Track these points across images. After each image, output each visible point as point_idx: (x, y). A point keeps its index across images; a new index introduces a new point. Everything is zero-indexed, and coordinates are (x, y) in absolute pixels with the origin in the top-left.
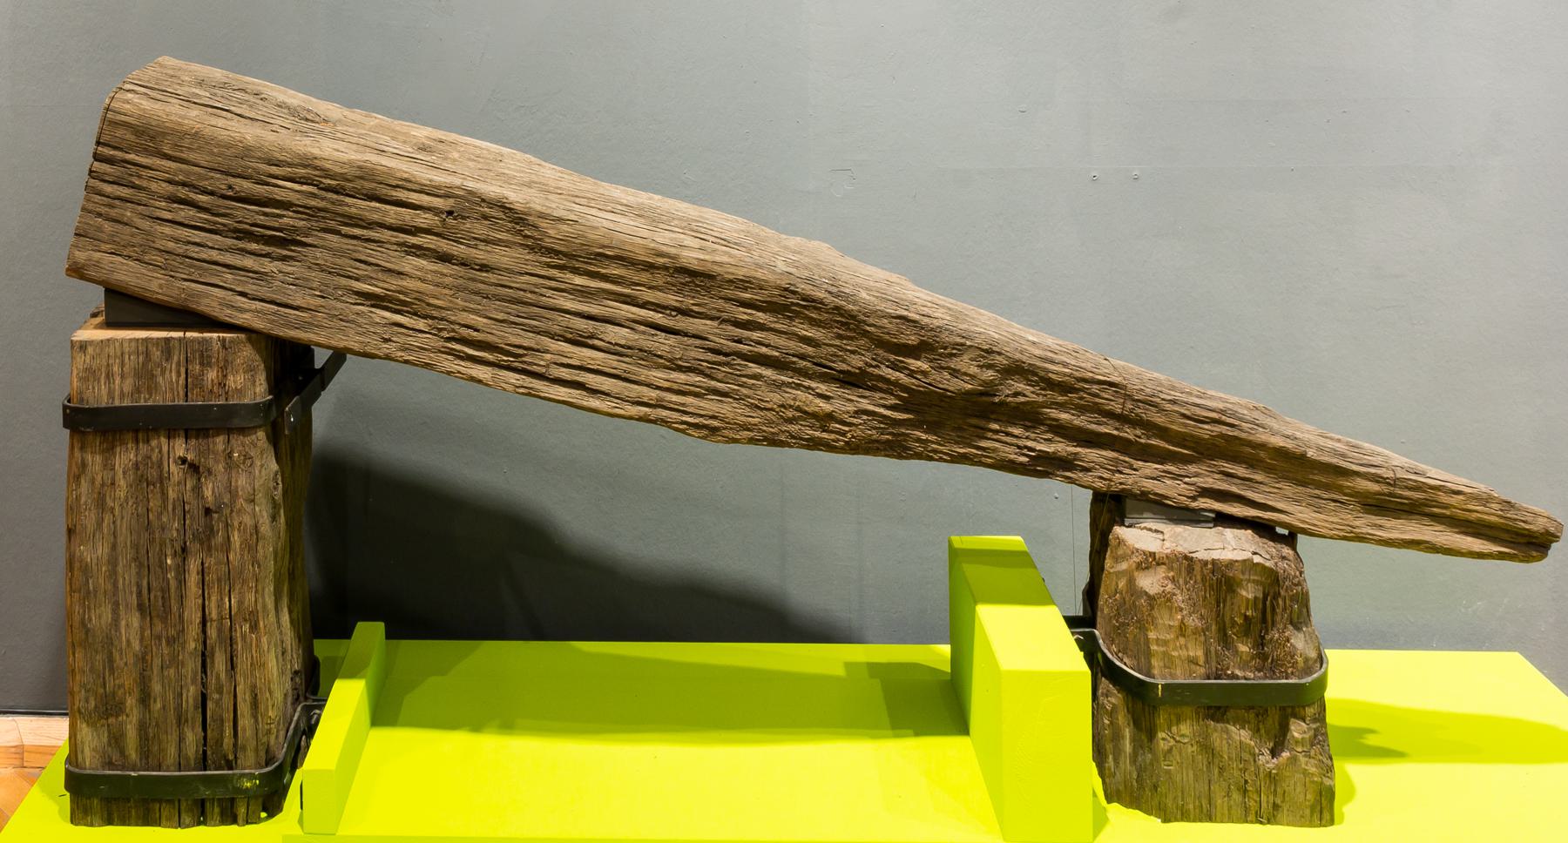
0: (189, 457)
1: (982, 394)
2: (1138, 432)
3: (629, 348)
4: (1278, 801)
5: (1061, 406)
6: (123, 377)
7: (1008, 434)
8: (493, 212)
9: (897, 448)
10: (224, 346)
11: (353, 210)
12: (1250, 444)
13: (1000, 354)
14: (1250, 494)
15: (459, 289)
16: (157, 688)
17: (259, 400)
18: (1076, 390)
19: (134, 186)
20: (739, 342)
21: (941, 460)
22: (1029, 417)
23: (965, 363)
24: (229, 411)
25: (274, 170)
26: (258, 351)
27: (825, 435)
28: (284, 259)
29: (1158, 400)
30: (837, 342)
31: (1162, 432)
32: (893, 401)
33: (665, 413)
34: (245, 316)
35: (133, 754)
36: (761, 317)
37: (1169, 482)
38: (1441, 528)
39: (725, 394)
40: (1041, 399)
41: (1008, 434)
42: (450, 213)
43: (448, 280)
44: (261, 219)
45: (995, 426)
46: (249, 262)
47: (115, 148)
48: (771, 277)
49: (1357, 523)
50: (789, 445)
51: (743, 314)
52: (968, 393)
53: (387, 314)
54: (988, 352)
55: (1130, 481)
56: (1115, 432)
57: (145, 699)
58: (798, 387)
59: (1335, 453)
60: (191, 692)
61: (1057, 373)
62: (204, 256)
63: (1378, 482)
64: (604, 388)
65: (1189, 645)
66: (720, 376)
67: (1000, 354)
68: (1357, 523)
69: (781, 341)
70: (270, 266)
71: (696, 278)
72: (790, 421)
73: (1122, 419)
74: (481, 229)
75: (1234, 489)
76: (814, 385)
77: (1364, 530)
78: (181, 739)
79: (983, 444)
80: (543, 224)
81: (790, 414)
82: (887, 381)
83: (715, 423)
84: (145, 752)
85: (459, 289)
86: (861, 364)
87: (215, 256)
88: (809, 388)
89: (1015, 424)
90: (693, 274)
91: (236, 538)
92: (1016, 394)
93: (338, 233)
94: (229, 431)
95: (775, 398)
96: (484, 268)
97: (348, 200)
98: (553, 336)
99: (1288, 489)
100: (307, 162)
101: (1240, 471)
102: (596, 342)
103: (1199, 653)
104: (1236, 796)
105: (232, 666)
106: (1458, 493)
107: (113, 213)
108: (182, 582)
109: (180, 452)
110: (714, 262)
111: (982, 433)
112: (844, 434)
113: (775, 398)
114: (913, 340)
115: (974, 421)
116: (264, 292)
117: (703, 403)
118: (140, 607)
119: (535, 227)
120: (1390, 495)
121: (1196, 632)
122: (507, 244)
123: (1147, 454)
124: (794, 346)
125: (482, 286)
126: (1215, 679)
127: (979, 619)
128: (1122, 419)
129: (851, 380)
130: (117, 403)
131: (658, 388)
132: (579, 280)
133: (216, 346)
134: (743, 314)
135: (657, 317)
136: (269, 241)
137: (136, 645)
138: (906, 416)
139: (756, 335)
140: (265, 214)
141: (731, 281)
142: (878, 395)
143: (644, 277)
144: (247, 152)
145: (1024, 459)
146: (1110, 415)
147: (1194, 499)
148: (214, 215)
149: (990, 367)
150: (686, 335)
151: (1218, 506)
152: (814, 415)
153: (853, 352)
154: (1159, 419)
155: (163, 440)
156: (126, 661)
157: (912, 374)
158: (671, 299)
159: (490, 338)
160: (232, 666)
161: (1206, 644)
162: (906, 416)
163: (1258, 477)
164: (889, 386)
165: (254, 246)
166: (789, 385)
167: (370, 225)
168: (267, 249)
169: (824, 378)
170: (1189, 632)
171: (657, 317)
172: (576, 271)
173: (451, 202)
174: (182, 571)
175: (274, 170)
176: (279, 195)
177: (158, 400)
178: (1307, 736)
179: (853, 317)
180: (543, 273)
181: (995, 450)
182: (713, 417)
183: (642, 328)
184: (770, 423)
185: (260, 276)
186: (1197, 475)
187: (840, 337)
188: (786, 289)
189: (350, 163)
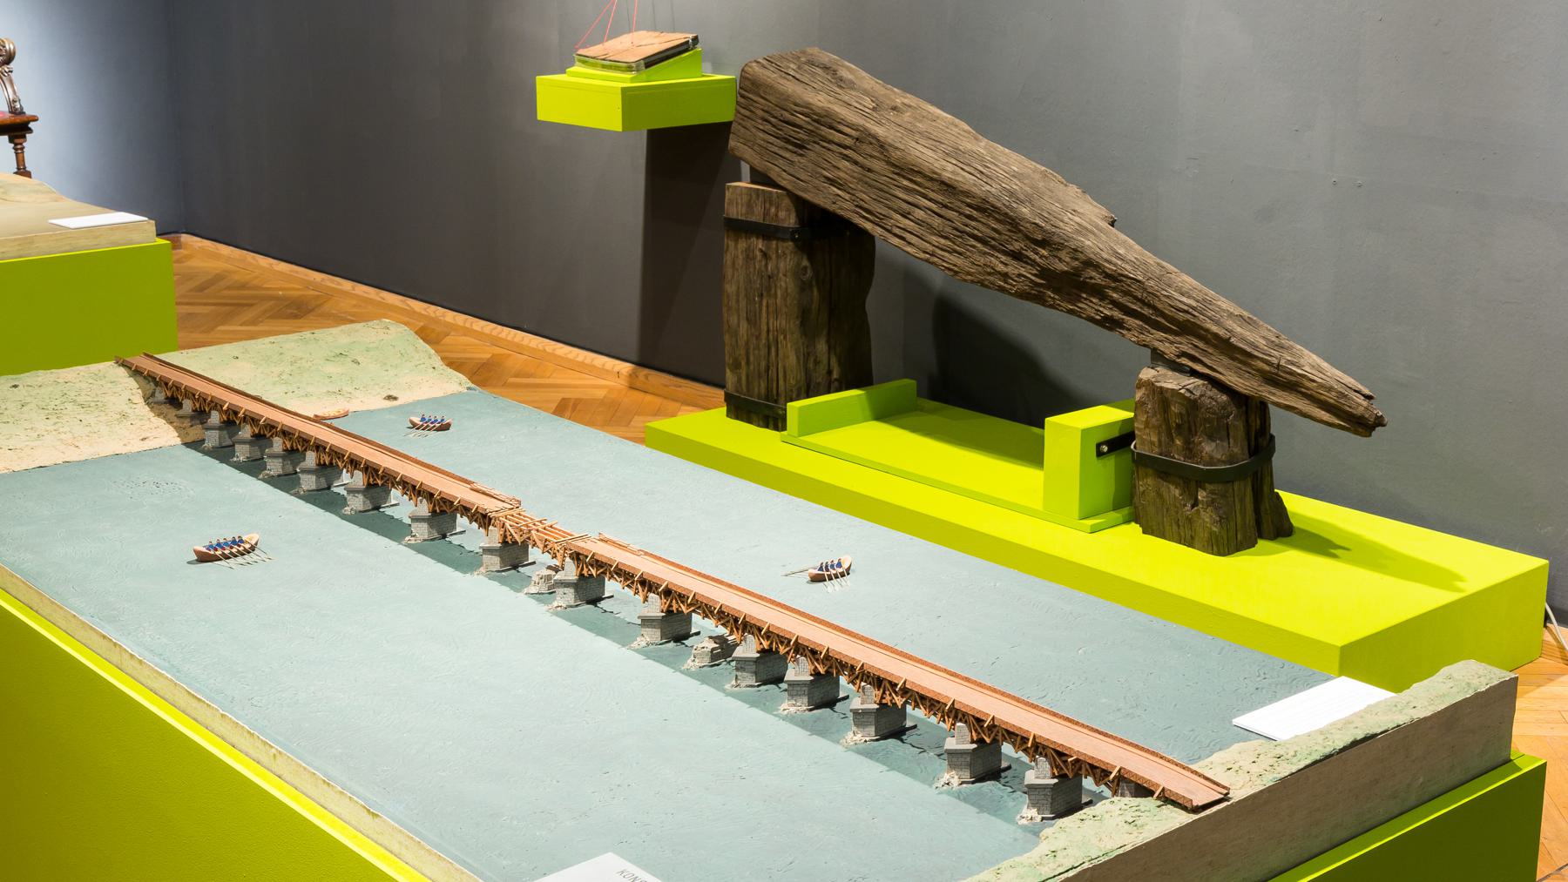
0: (764, 249)
1: (1074, 275)
2: (1151, 312)
3: (924, 222)
4: (1193, 534)
5: (1114, 289)
6: (742, 205)
7: (1091, 302)
8: (874, 141)
9: (1039, 299)
10: (778, 197)
11: (823, 133)
12: (1202, 328)
13: (1082, 253)
14: (1204, 359)
15: (860, 180)
16: (752, 359)
17: (791, 226)
18: (1120, 281)
19: (751, 111)
20: (966, 226)
21: (1062, 310)
22: (1098, 292)
23: (1063, 254)
24: (777, 229)
25: (797, 108)
26: (792, 202)
27: (1006, 285)
28: (801, 155)
29: (1158, 294)
30: (1007, 233)
31: (1163, 315)
32: (1035, 272)
33: (936, 259)
34: (784, 182)
35: (745, 390)
36: (975, 213)
37: (1167, 344)
38: (1308, 402)
39: (960, 254)
40: (1103, 283)
41: (1091, 302)
42: (857, 139)
43: (855, 175)
44: (792, 133)
45: (1084, 296)
46: (787, 155)
47: (745, 91)
48: (978, 192)
49: (1260, 389)
50: (989, 288)
51: (968, 211)
52: (1066, 272)
53: (835, 189)
54: (1076, 250)
55: (1148, 340)
56: (1139, 310)
57: (748, 363)
58: (992, 256)
59: (1252, 344)
60: (763, 364)
61: (1109, 269)
62: (773, 150)
63: (1269, 365)
64: (912, 242)
65: (1151, 433)
66: (958, 243)
67: (1082, 253)
68: (1260, 389)
69: (984, 229)
70: (796, 159)
71: (948, 187)
72: (989, 274)
73: (1141, 301)
74: (869, 150)
75: (1197, 355)
76: (999, 256)
77: (1264, 394)
78: (760, 385)
79: (1080, 305)
80: (890, 149)
81: (989, 270)
82: (1030, 259)
83: (956, 269)
84: (748, 390)
85: (860, 180)
86: (1019, 248)
87: (775, 149)
88: (997, 257)
89: (1094, 297)
90: (948, 185)
91: (779, 293)
92: (1091, 278)
93: (818, 144)
94: (778, 239)
95: (982, 260)
96: (869, 170)
97: (822, 128)
98: (895, 211)
99: (1226, 360)
100: (808, 106)
101: (1201, 344)
102: (910, 217)
103: (1155, 439)
104: (1175, 527)
105: (777, 355)
106: (1314, 381)
107: (744, 123)
108: (761, 310)
109: (760, 246)
110: (956, 181)
111: (1079, 299)
112: (1014, 286)
113: (982, 260)
114: (1039, 237)
115: (1074, 291)
116: (791, 171)
117: (951, 257)
118: (747, 319)
119: (887, 150)
120: (1276, 374)
121: (1154, 427)
122: (879, 159)
123: (1158, 326)
124: (988, 231)
125: (868, 180)
126: (1166, 456)
127: (1360, 715)
128: (1141, 301)
129: (1017, 256)
130: (740, 218)
131: (934, 246)
132: (906, 183)
133: (775, 196)
134: (968, 211)
135: (933, 206)
136: (796, 145)
137: (745, 338)
138: (1042, 282)
139: (973, 223)
140: (794, 131)
141: (962, 192)
142: (1029, 267)
143: (929, 184)
144: (787, 98)
145: (1098, 317)
146: (1136, 298)
147: (1178, 357)
148: (778, 129)
149: (1077, 259)
150: (945, 218)
151: (1190, 364)
152: (999, 273)
153: (1016, 240)
154: (1160, 306)
155: (755, 239)
156: (742, 342)
157: (1041, 257)
158: (939, 198)
159: (871, 208)
160: (777, 355)
161: (1159, 433)
162: (1042, 282)
163: (1210, 351)
164: (1034, 263)
165: (790, 147)
166: (989, 254)
167: (830, 142)
168: (796, 150)
169: (1005, 253)
170: (1150, 426)
171: (933, 206)
172: (904, 177)
173: (858, 133)
174: (761, 304)
175: (797, 108)
176: (798, 122)
177: (753, 219)
178: (1205, 500)
179: (1013, 220)
180: (891, 176)
181: (1085, 309)
182: (955, 265)
183: (929, 212)
184: (980, 273)
185: (792, 162)
186: (1181, 343)
187: (1009, 230)
188: (984, 200)
189: (822, 108)
